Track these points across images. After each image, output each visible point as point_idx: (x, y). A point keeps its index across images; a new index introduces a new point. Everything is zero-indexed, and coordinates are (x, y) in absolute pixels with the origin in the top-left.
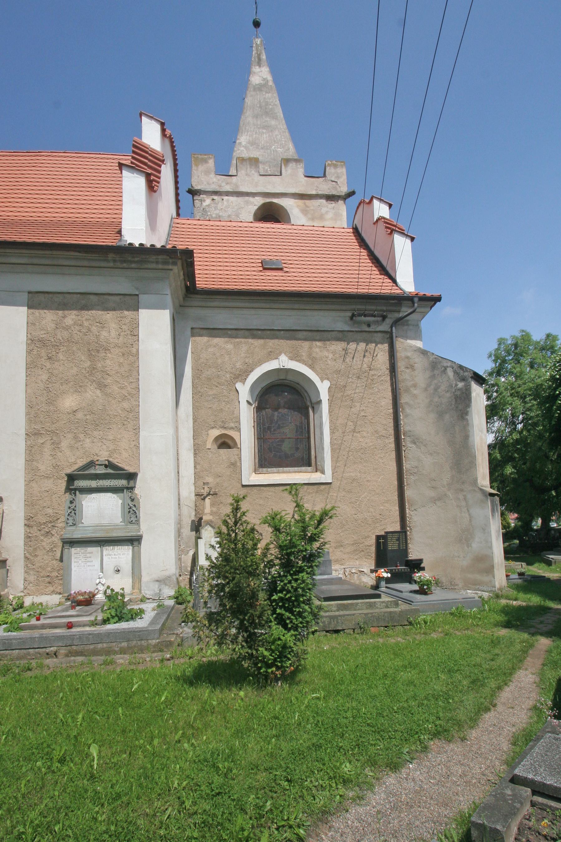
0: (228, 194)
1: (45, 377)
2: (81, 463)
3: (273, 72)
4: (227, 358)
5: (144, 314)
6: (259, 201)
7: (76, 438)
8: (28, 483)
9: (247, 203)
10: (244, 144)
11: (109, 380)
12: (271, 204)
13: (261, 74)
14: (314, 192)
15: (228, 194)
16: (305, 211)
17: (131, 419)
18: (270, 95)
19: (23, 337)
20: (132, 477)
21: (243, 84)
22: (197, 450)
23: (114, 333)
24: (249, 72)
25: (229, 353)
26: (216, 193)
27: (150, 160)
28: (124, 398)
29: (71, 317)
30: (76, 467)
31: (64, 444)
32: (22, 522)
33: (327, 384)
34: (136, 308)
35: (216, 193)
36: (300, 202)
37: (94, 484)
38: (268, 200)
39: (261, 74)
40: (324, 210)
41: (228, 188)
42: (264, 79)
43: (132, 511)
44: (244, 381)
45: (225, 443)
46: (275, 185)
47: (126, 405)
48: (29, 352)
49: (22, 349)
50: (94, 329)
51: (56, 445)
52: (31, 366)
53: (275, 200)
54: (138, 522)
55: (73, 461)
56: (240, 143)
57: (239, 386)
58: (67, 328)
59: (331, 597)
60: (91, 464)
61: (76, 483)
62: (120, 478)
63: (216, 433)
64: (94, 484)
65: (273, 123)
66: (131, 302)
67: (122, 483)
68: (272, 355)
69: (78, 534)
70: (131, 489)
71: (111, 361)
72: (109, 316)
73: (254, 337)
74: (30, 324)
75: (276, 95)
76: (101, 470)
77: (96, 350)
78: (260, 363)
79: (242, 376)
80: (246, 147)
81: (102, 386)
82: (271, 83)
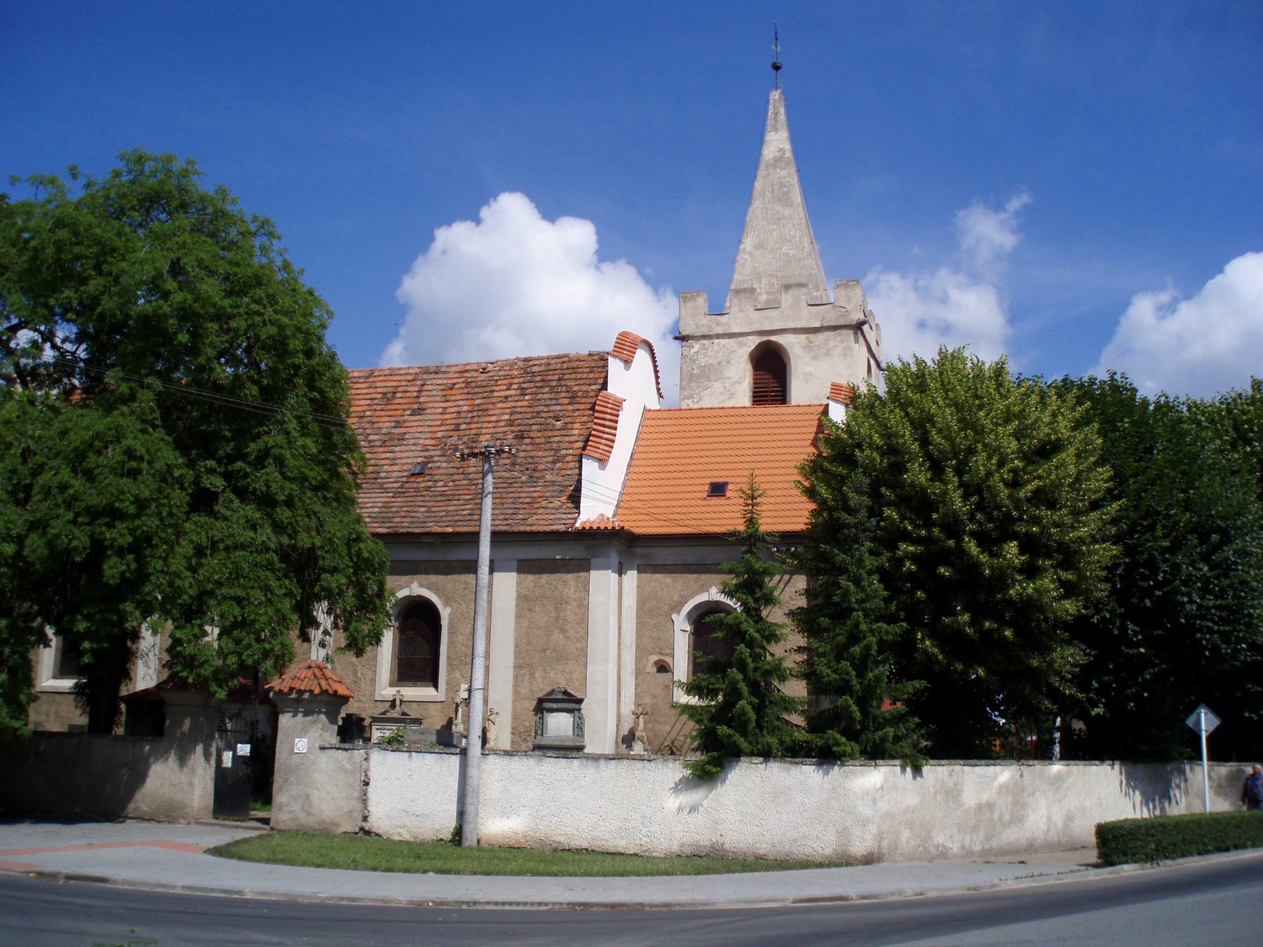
0: (718, 336)
1: (526, 624)
2: (548, 689)
3: (794, 139)
4: (665, 592)
5: (594, 575)
6: (753, 342)
7: (545, 670)
8: (514, 702)
9: (741, 345)
10: (748, 249)
11: (568, 627)
12: (768, 342)
13: (777, 142)
14: (818, 325)
15: (718, 336)
16: (808, 347)
17: (582, 656)
18: (784, 173)
19: (514, 595)
20: (580, 701)
21: (759, 142)
22: (639, 672)
23: (572, 589)
24: (760, 142)
25: (667, 587)
26: (705, 337)
27: (604, 426)
28: (578, 640)
29: (545, 578)
30: (544, 692)
31: (538, 675)
32: (510, 730)
33: (448, 610)
34: (588, 571)
35: (705, 337)
36: (803, 337)
37: (555, 706)
38: (765, 339)
39: (777, 142)
40: (831, 344)
41: (719, 330)
42: (780, 150)
43: (579, 727)
44: (679, 612)
45: (663, 668)
46: (773, 321)
47: (579, 645)
48: (517, 605)
49: (514, 602)
50: (560, 587)
51: (532, 675)
52: (519, 616)
53: (773, 338)
54: (583, 736)
55: (542, 689)
56: (744, 249)
57: (674, 616)
58: (541, 587)
59: (1067, 913)
60: (553, 692)
61: (542, 706)
62: (570, 702)
63: (655, 658)
64: (555, 706)
65: (787, 212)
66: (583, 566)
67: (573, 706)
68: (704, 588)
69: (544, 741)
70: (579, 710)
71: (570, 612)
72: (570, 576)
73: (691, 572)
74: (519, 584)
75: (793, 170)
76: (560, 696)
77: (560, 603)
78: (693, 595)
79: (677, 608)
80: (750, 253)
81: (563, 631)
82: (788, 154)
